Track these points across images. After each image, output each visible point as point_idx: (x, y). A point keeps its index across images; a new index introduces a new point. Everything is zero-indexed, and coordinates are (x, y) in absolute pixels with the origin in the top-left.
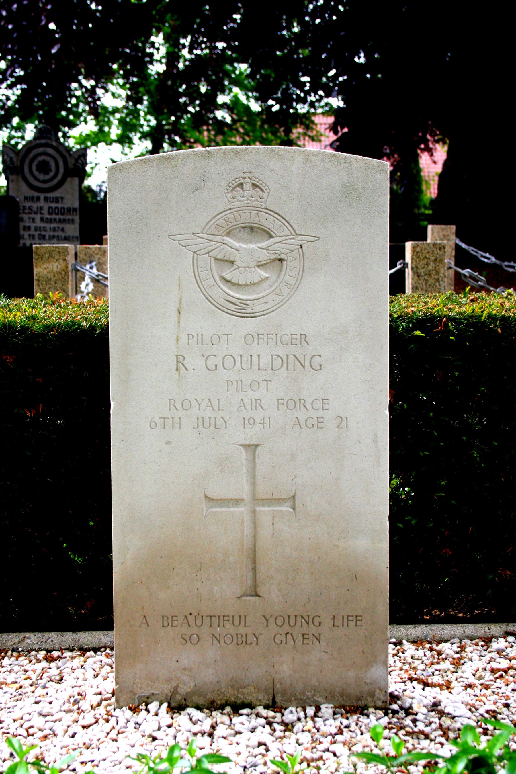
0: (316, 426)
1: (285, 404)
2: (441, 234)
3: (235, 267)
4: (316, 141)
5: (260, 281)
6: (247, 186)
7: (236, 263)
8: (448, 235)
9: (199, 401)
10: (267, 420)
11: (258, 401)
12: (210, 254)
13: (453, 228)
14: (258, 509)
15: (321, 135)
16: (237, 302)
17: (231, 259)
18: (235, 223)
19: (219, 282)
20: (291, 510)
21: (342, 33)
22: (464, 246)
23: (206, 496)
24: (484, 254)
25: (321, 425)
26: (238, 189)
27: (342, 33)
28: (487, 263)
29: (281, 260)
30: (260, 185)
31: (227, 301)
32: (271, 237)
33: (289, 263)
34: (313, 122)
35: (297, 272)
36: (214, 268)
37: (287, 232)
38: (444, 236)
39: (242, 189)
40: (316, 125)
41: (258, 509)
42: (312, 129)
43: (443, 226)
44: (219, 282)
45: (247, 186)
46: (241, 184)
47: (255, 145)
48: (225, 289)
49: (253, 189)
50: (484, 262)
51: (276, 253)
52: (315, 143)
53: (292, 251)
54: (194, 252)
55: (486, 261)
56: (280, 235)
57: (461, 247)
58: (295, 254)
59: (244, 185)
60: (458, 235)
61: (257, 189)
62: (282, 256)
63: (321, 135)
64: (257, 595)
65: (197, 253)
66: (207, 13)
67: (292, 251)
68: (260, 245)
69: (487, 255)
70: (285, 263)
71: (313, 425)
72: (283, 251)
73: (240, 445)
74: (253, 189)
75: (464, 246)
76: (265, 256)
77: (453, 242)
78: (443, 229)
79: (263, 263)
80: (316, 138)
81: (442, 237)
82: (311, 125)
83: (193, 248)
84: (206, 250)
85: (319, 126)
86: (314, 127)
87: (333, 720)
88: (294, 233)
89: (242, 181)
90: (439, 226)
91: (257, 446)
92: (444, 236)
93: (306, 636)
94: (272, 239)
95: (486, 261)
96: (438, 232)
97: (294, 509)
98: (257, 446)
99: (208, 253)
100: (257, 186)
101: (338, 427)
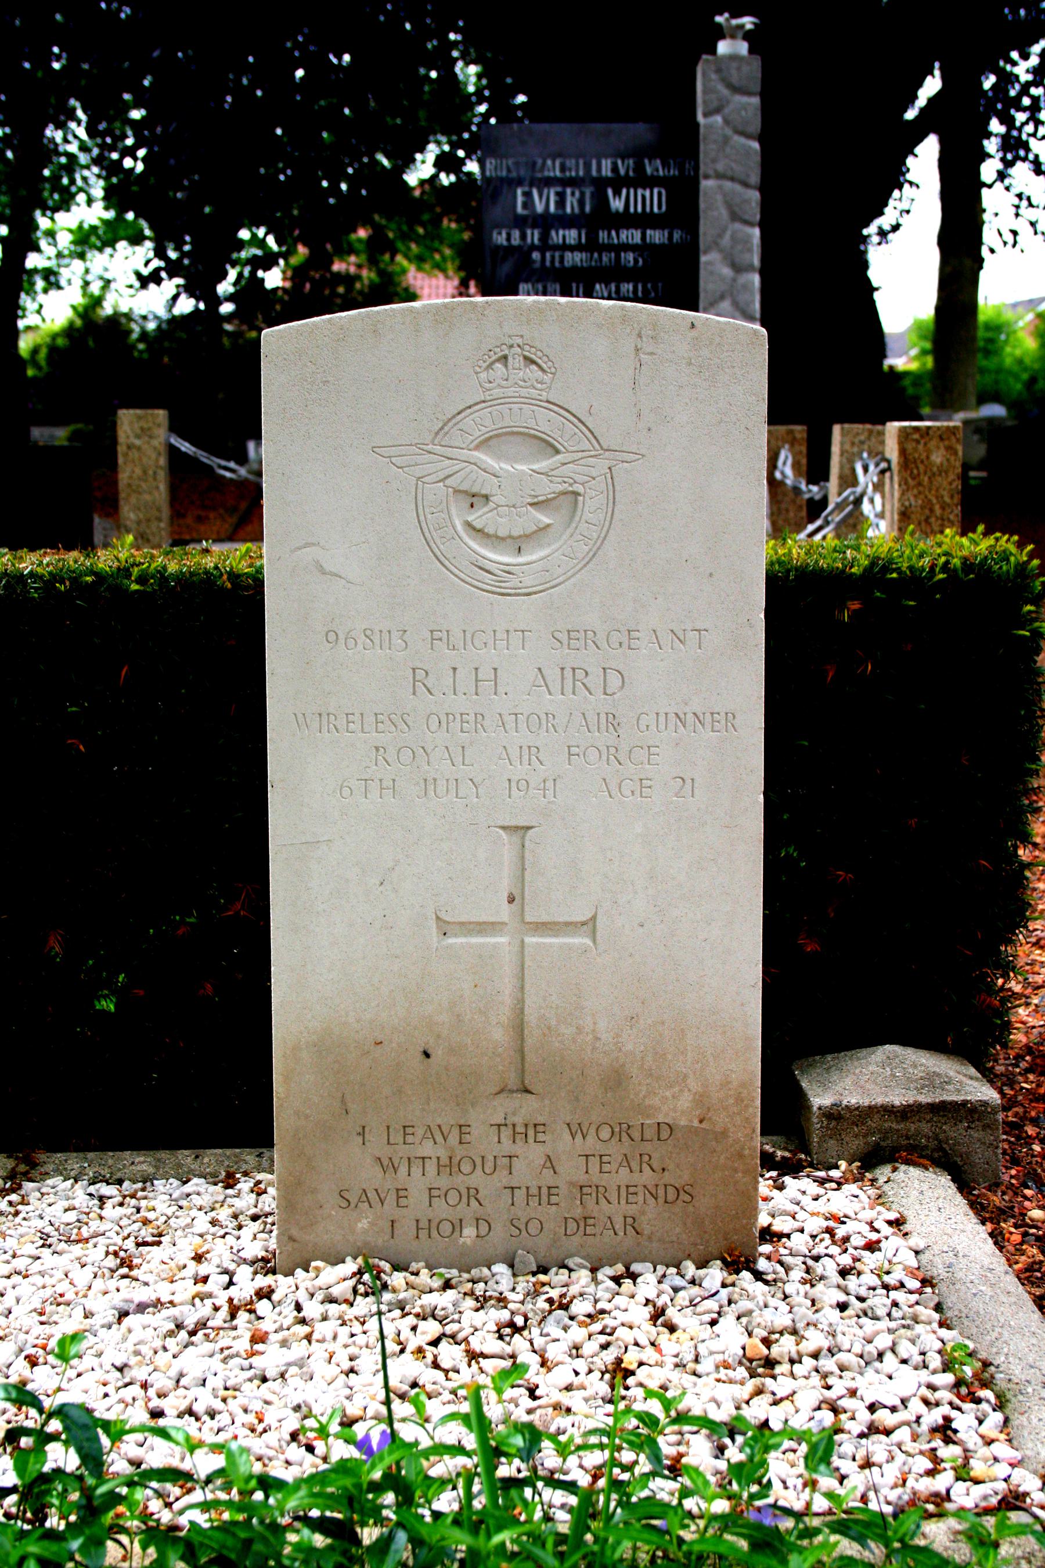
2: (136, 426)
3: (492, 505)
5: (535, 532)
6: (515, 361)
8: (149, 429)
11: (534, 750)
12: (448, 482)
13: (162, 414)
14: (528, 940)
16: (491, 567)
21: (156, 54)
22: (185, 447)
24: (223, 463)
26: (498, 365)
27: (156, 54)
28: (231, 480)
29: (576, 494)
30: (539, 361)
35: (602, 516)
38: (142, 429)
41: (528, 940)
43: (139, 412)
45: (515, 361)
46: (505, 357)
47: (589, 294)
50: (224, 477)
55: (228, 474)
57: (178, 449)
59: (510, 359)
60: (175, 427)
61: (534, 367)
62: (579, 488)
64: (527, 1091)
66: (306, 31)
69: (232, 465)
72: (577, 477)
73: (503, 828)
74: (526, 366)
75: (185, 447)
76: (547, 489)
77: (162, 439)
78: (139, 418)
79: (541, 498)
81: (139, 431)
83: (418, 471)
87: (650, 1298)
90: (132, 411)
91: (529, 828)
92: (142, 429)
93: (605, 1159)
94: (559, 457)
95: (228, 474)
96: (131, 423)
100: (533, 362)
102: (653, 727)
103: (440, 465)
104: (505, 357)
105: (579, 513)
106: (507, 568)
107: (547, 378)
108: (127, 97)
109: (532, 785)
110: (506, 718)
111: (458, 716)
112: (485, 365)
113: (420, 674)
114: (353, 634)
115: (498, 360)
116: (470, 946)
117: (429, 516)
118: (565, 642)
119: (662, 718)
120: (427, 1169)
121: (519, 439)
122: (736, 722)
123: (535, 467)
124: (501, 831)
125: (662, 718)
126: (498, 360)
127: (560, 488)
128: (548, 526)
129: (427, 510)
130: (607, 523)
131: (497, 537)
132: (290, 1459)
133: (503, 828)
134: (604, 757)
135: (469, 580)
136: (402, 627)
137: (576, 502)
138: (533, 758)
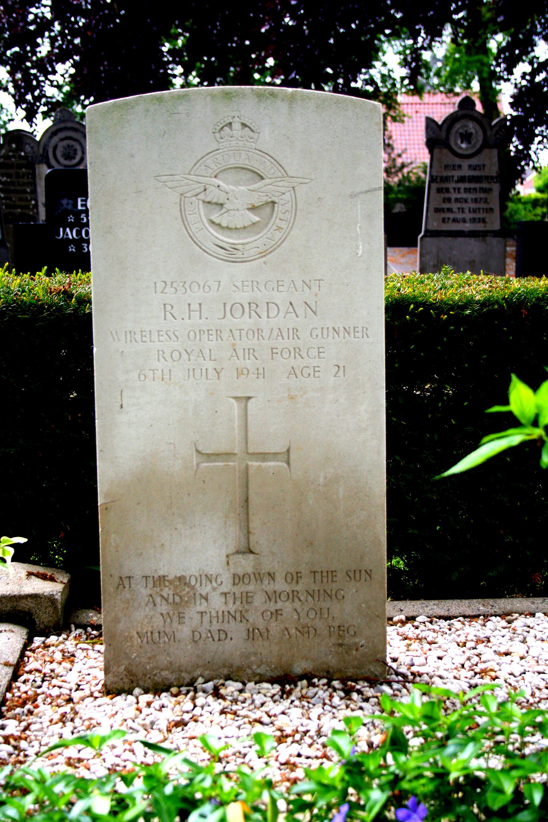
0: (312, 375)
1: (279, 353)
3: (224, 210)
4: (398, 122)
6: (237, 126)
7: (225, 206)
9: (189, 351)
10: (261, 371)
11: (251, 351)
12: (198, 197)
15: (404, 116)
17: (220, 202)
18: (224, 164)
19: (207, 225)
20: (285, 465)
23: (198, 451)
25: (317, 374)
29: (274, 203)
31: (218, 246)
32: (262, 178)
33: (280, 206)
34: (396, 102)
36: (202, 210)
37: (280, 174)
39: (231, 128)
40: (399, 104)
42: (395, 108)
44: (207, 225)
45: (237, 126)
46: (231, 123)
48: (212, 231)
49: (242, 129)
51: (267, 196)
52: (397, 124)
53: (284, 194)
54: (182, 194)
56: (271, 176)
58: (287, 197)
59: (233, 124)
61: (247, 129)
62: (274, 199)
63: (404, 116)
64: (251, 552)
65: (185, 195)
67: (284, 194)
68: (249, 187)
70: (276, 205)
71: (309, 374)
73: (235, 398)
76: (257, 200)
80: (398, 119)
82: (393, 105)
84: (194, 193)
85: (402, 106)
86: (397, 107)
88: (285, 175)
89: (231, 120)
91: (249, 398)
94: (263, 181)
97: (288, 463)
98: (249, 398)
99: (197, 195)
101: (335, 376)
102: (320, 335)
103: (193, 186)
104: (231, 123)
105: (275, 213)
106: (232, 246)
107: (255, 136)
108: (311, 20)
109: (251, 372)
110: (234, 332)
111: (206, 332)
112: (219, 128)
113: (168, 308)
114: (208, 283)
115: (226, 126)
116: (216, 466)
117: (188, 216)
118: (241, 288)
119: (325, 331)
120: (316, 577)
121: (233, 171)
122: (368, 332)
123: (249, 187)
124: (233, 401)
125: (325, 331)
126: (226, 126)
127: (264, 199)
128: (258, 222)
129: (187, 213)
130: (292, 219)
131: (236, 228)
132: (335, 719)
133: (235, 398)
134: (292, 354)
135: (215, 255)
136: (183, 280)
137: (274, 206)
138: (297, 354)
